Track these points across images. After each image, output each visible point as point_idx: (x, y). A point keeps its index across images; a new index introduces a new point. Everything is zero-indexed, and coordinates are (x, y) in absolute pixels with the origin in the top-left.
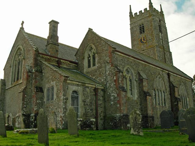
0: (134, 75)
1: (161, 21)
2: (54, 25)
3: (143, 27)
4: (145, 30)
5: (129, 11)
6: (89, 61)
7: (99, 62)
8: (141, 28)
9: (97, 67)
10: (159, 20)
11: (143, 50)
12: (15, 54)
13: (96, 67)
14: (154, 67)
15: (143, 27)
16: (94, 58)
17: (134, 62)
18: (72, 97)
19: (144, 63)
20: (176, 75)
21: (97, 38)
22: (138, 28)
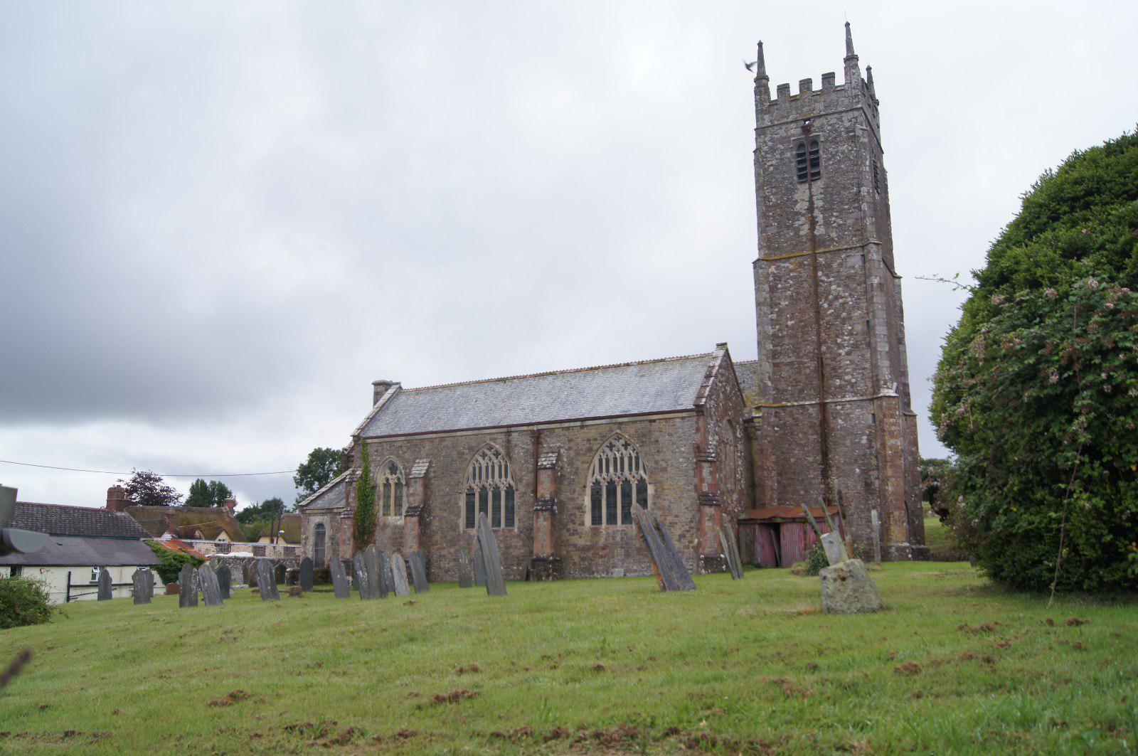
19: (434, 436)
20: (578, 424)
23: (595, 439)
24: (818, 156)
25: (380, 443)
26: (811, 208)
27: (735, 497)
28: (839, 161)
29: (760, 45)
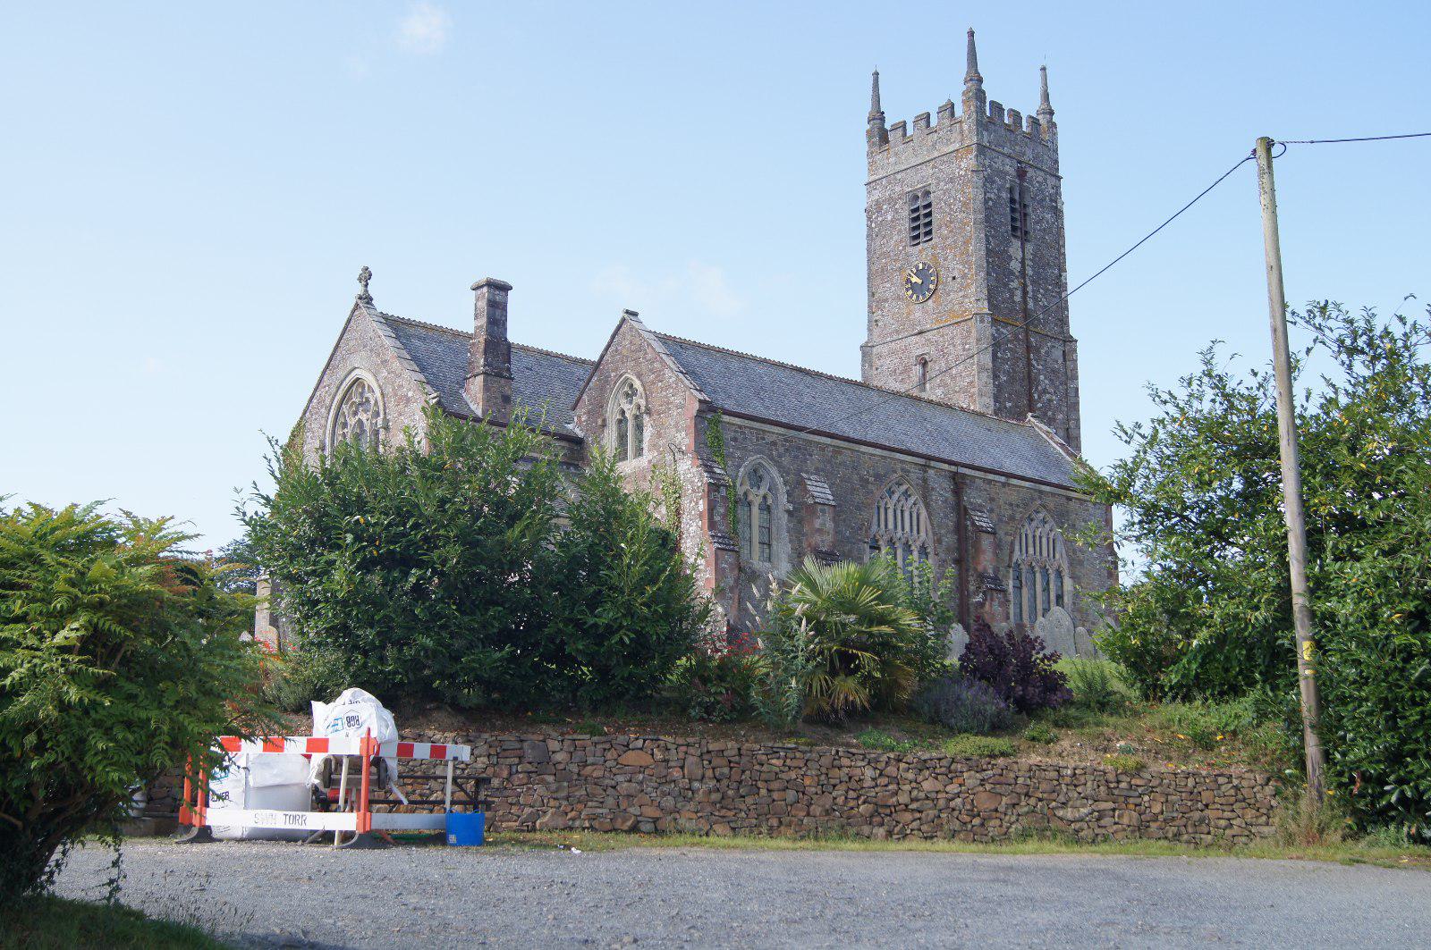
0: (782, 489)
1: (1030, 173)
2: (496, 295)
3: (929, 205)
4: (934, 226)
5: (867, 107)
6: (622, 438)
7: (654, 446)
8: (917, 210)
9: (650, 462)
10: (1012, 171)
11: (920, 333)
12: (339, 397)
13: (643, 462)
14: (878, 452)
15: (929, 205)
16: (639, 428)
17: (786, 440)
18: (1287, 624)
19: (828, 441)
20: (1003, 479)
21: (649, 356)
22: (905, 213)
23: (1018, 506)
24: (1002, 210)
25: (740, 427)
26: (1023, 273)
27: (186, 724)
28: (1044, 230)
29: (971, 34)
